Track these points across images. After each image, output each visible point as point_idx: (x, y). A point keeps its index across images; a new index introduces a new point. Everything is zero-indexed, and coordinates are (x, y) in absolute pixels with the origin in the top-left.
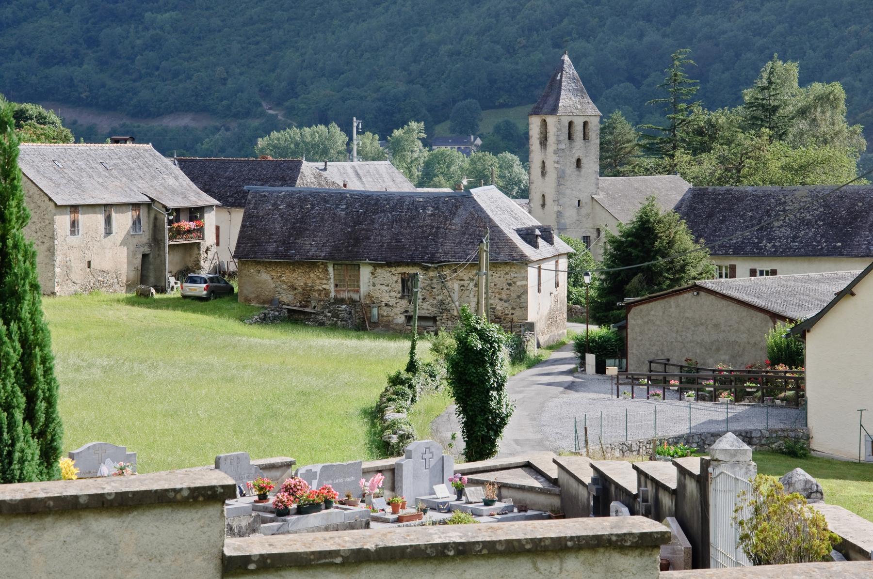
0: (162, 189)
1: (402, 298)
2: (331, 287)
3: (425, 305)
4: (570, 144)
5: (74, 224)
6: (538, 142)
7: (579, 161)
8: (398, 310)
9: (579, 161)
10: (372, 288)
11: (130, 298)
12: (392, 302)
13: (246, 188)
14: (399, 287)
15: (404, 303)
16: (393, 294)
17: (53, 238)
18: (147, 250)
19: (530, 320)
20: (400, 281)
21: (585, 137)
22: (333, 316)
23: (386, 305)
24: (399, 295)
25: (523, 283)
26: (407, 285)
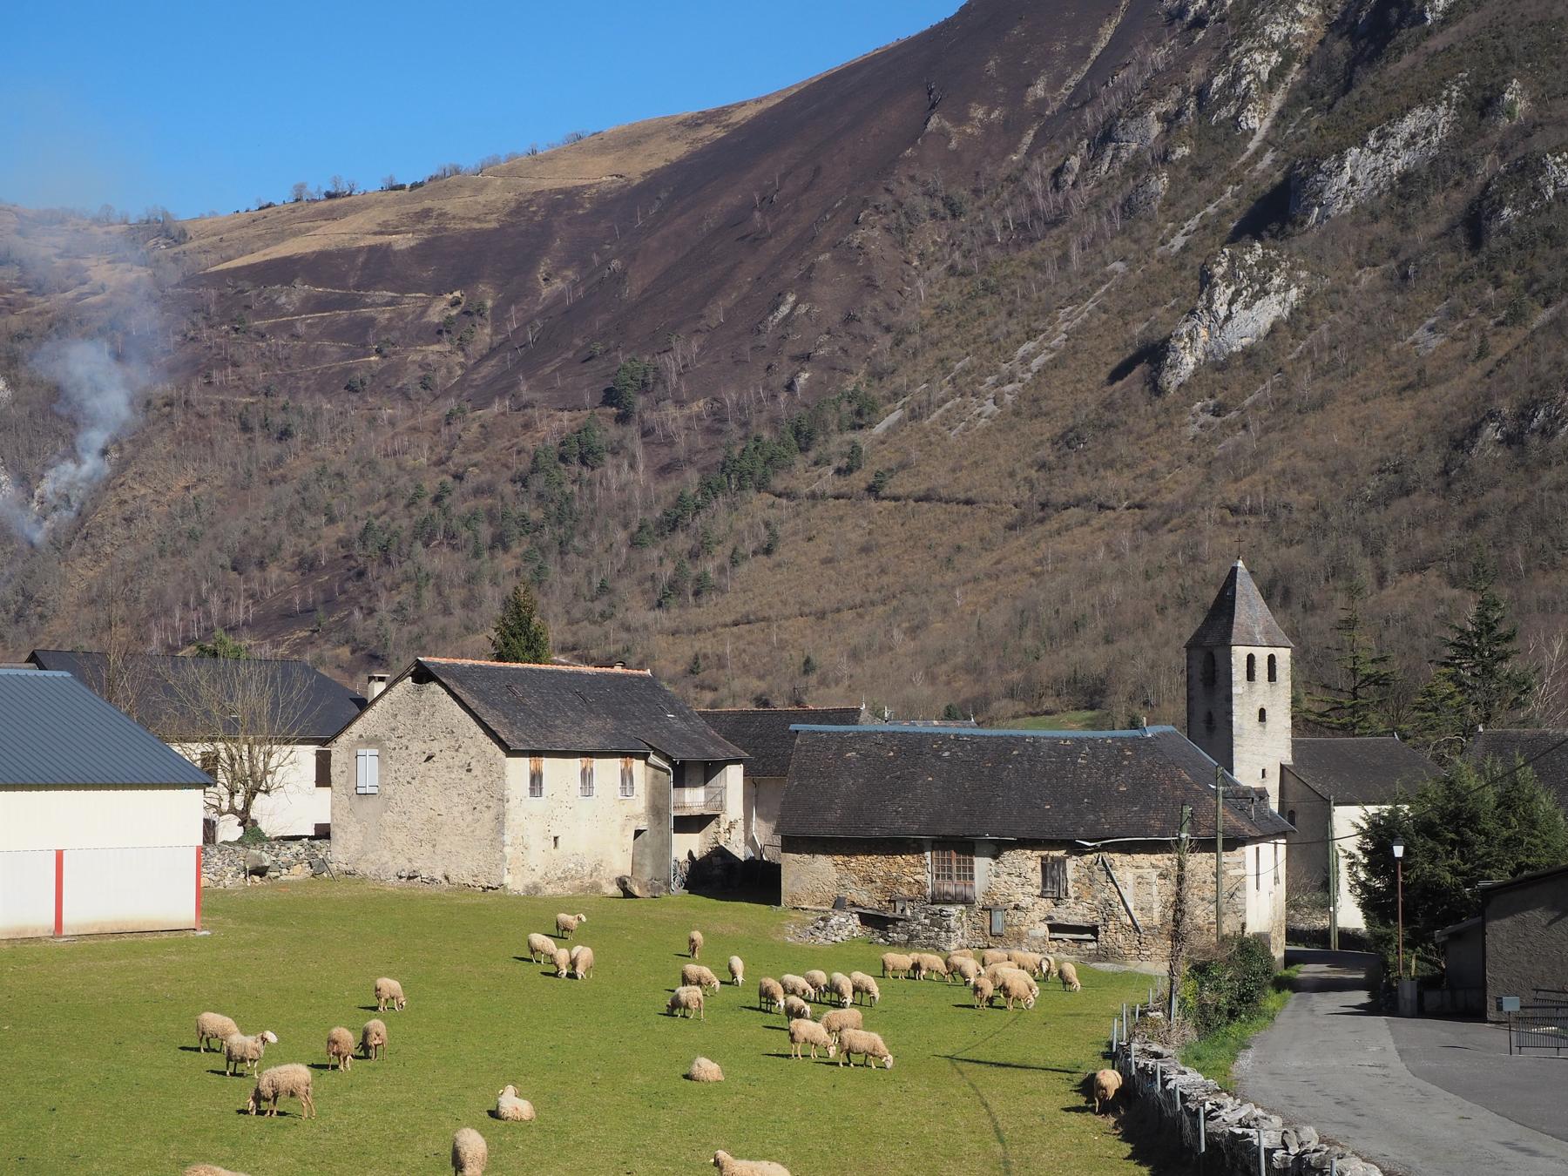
0: (665, 734)
1: (1041, 896)
2: (927, 878)
3: (1080, 909)
4: (1251, 687)
5: (536, 778)
6: (1201, 685)
7: (1262, 713)
8: (1037, 915)
9: (1262, 713)
10: (994, 879)
11: (1048, 84)
12: (1026, 902)
13: (792, 727)
14: (1037, 878)
15: (1046, 903)
16: (1029, 889)
17: (503, 800)
18: (643, 825)
19: (1252, 929)
20: (1039, 868)
21: (1272, 676)
22: (932, 924)
23: (1016, 908)
24: (1038, 892)
25: (1240, 872)
26: (1052, 874)
